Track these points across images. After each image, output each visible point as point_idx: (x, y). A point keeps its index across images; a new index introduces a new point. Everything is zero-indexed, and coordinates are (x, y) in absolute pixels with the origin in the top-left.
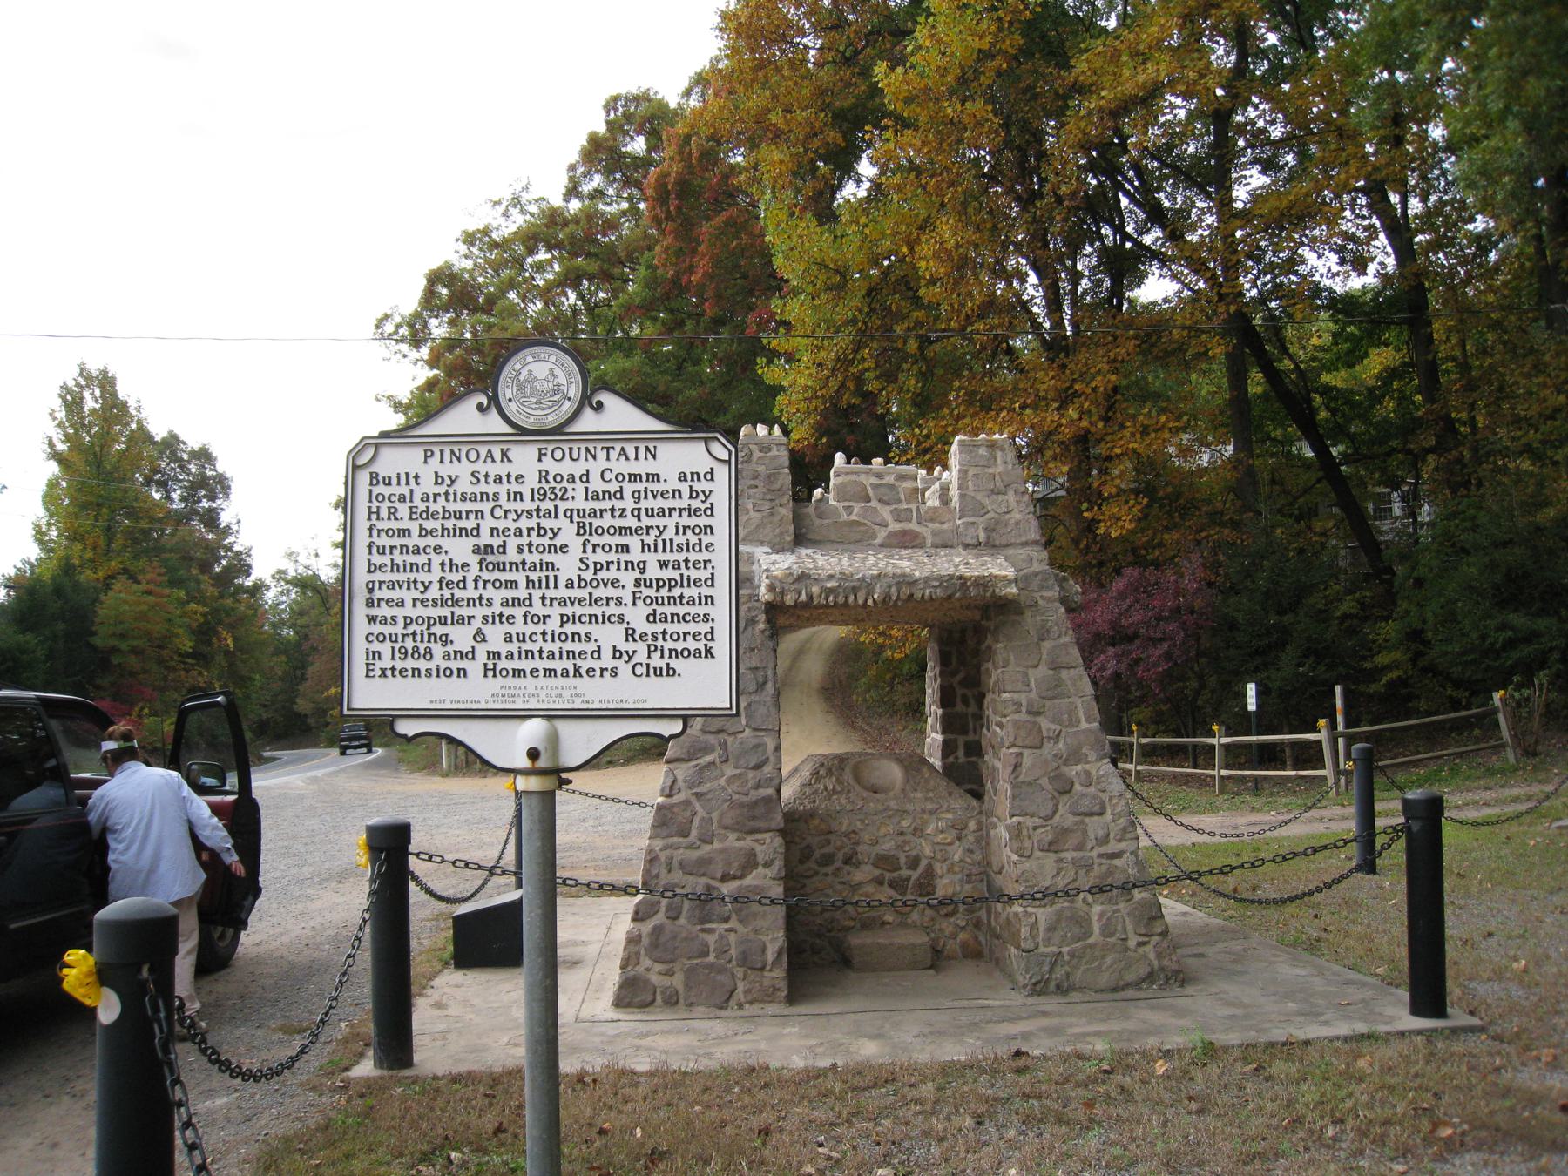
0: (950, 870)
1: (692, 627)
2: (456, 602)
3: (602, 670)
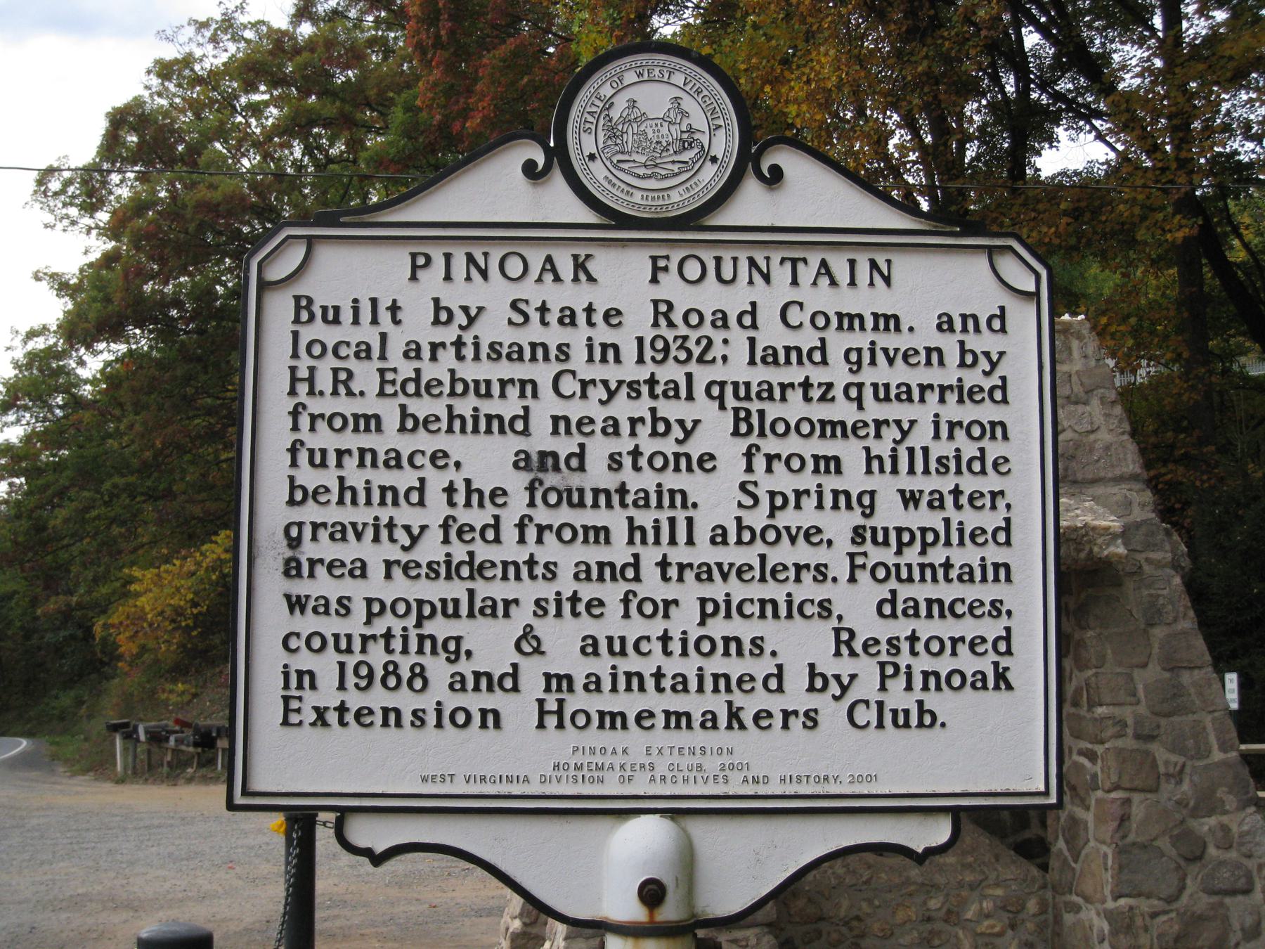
1: (968, 628)
2: (479, 570)
3: (786, 714)
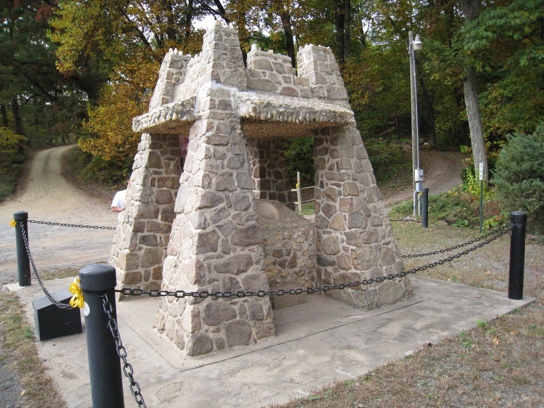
0: (303, 255)
